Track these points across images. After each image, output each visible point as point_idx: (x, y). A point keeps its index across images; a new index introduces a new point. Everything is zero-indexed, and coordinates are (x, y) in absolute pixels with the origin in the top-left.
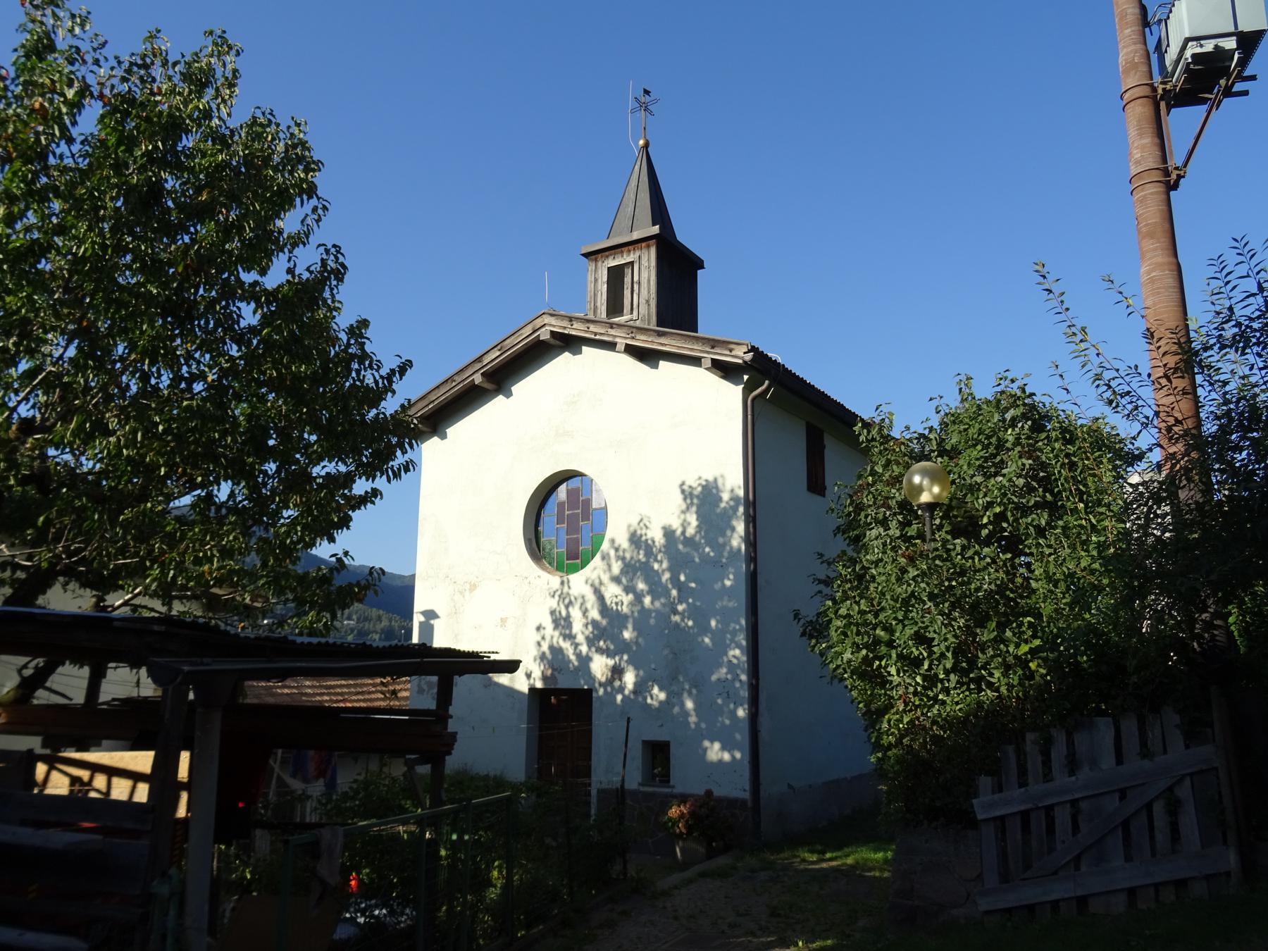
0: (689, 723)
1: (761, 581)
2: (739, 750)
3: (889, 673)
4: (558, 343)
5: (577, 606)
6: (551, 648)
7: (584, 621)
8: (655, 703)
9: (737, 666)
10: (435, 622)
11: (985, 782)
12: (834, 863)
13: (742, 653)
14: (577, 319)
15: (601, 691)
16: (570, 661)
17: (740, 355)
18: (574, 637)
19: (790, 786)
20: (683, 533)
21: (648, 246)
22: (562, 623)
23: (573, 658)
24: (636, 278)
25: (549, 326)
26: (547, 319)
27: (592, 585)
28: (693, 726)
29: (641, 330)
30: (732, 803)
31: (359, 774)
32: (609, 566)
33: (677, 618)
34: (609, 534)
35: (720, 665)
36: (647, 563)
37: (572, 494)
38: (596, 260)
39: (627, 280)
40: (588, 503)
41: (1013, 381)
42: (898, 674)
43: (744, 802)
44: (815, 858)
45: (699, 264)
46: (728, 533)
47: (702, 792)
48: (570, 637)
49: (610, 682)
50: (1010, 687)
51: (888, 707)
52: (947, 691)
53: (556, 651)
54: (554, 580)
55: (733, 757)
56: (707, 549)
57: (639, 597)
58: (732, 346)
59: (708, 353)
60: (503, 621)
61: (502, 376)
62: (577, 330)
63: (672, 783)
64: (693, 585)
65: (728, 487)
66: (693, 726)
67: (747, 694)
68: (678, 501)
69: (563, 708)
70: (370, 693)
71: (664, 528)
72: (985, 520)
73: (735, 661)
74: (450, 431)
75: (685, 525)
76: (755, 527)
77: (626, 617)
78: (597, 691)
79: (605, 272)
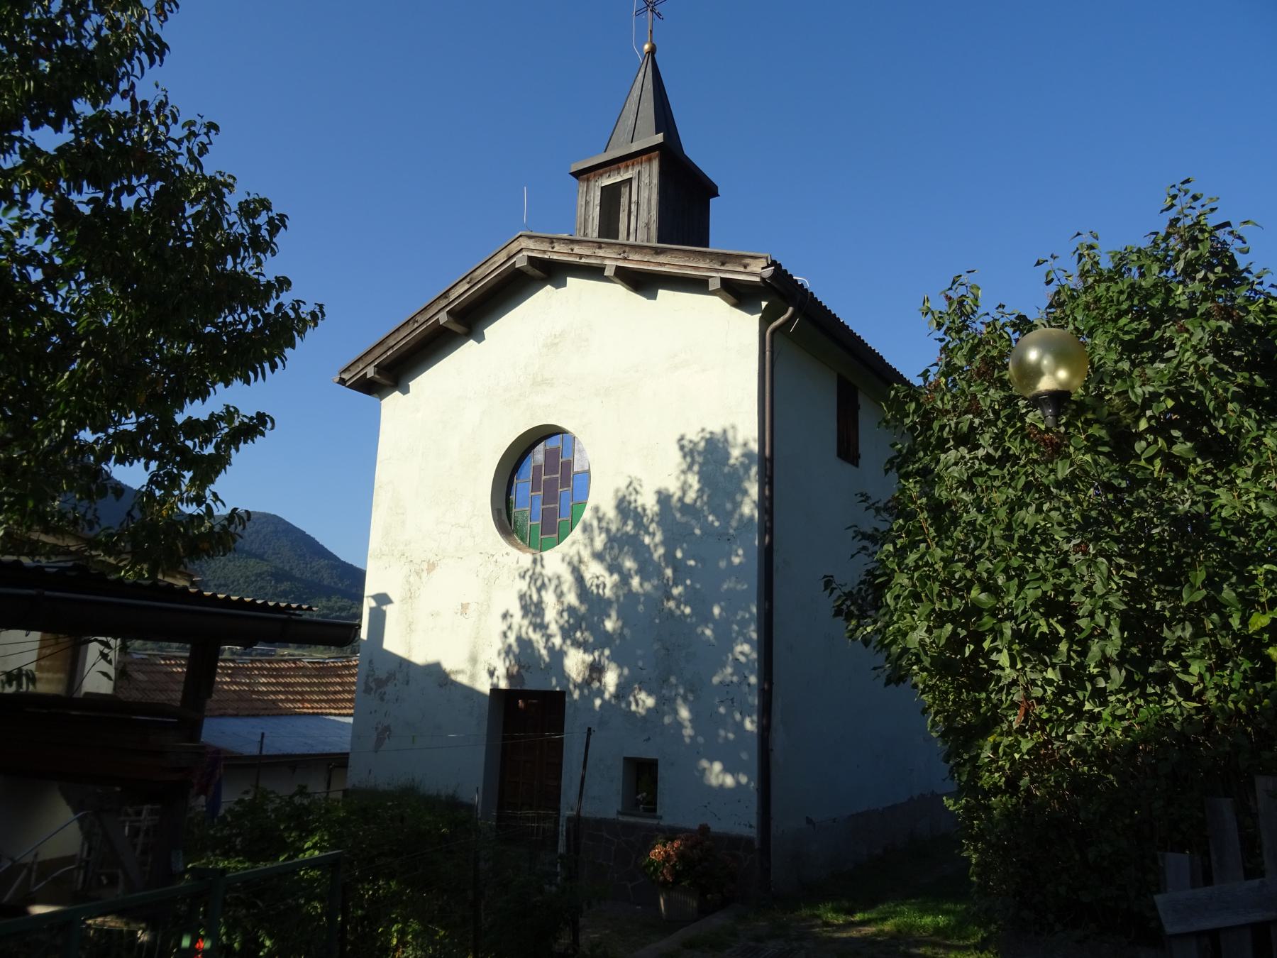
0: (683, 736)
3: (994, 665)
4: (537, 272)
5: (551, 589)
6: (519, 639)
7: (559, 607)
8: (642, 711)
10: (388, 609)
11: (1177, 864)
14: (559, 239)
15: (576, 695)
16: (540, 656)
17: (757, 271)
19: (809, 821)
20: (681, 499)
21: (650, 160)
22: (532, 609)
23: (544, 652)
24: (634, 198)
25: (527, 250)
26: (524, 243)
27: (569, 563)
28: (687, 740)
29: (635, 248)
30: (735, 843)
31: (246, 792)
32: (592, 540)
33: (672, 604)
34: (591, 503)
36: (636, 536)
37: (551, 455)
38: (588, 180)
39: (624, 201)
40: (568, 465)
41: (1195, 198)
42: (1013, 665)
43: (749, 841)
44: (841, 920)
45: (712, 191)
46: (738, 497)
48: (541, 627)
49: (587, 682)
50: (1225, 692)
51: (990, 722)
52: (1100, 696)
53: (525, 644)
54: (526, 559)
55: (738, 783)
56: (711, 518)
57: (625, 578)
58: (747, 261)
59: (717, 271)
60: (464, 607)
62: (559, 253)
63: (659, 813)
64: (692, 563)
65: (740, 440)
66: (687, 740)
67: (756, 702)
69: (528, 712)
70: (335, 693)
71: (659, 493)
72: (1143, 425)
73: (742, 659)
74: (489, 331)
75: (684, 488)
77: (609, 602)
78: (571, 694)
79: (598, 193)
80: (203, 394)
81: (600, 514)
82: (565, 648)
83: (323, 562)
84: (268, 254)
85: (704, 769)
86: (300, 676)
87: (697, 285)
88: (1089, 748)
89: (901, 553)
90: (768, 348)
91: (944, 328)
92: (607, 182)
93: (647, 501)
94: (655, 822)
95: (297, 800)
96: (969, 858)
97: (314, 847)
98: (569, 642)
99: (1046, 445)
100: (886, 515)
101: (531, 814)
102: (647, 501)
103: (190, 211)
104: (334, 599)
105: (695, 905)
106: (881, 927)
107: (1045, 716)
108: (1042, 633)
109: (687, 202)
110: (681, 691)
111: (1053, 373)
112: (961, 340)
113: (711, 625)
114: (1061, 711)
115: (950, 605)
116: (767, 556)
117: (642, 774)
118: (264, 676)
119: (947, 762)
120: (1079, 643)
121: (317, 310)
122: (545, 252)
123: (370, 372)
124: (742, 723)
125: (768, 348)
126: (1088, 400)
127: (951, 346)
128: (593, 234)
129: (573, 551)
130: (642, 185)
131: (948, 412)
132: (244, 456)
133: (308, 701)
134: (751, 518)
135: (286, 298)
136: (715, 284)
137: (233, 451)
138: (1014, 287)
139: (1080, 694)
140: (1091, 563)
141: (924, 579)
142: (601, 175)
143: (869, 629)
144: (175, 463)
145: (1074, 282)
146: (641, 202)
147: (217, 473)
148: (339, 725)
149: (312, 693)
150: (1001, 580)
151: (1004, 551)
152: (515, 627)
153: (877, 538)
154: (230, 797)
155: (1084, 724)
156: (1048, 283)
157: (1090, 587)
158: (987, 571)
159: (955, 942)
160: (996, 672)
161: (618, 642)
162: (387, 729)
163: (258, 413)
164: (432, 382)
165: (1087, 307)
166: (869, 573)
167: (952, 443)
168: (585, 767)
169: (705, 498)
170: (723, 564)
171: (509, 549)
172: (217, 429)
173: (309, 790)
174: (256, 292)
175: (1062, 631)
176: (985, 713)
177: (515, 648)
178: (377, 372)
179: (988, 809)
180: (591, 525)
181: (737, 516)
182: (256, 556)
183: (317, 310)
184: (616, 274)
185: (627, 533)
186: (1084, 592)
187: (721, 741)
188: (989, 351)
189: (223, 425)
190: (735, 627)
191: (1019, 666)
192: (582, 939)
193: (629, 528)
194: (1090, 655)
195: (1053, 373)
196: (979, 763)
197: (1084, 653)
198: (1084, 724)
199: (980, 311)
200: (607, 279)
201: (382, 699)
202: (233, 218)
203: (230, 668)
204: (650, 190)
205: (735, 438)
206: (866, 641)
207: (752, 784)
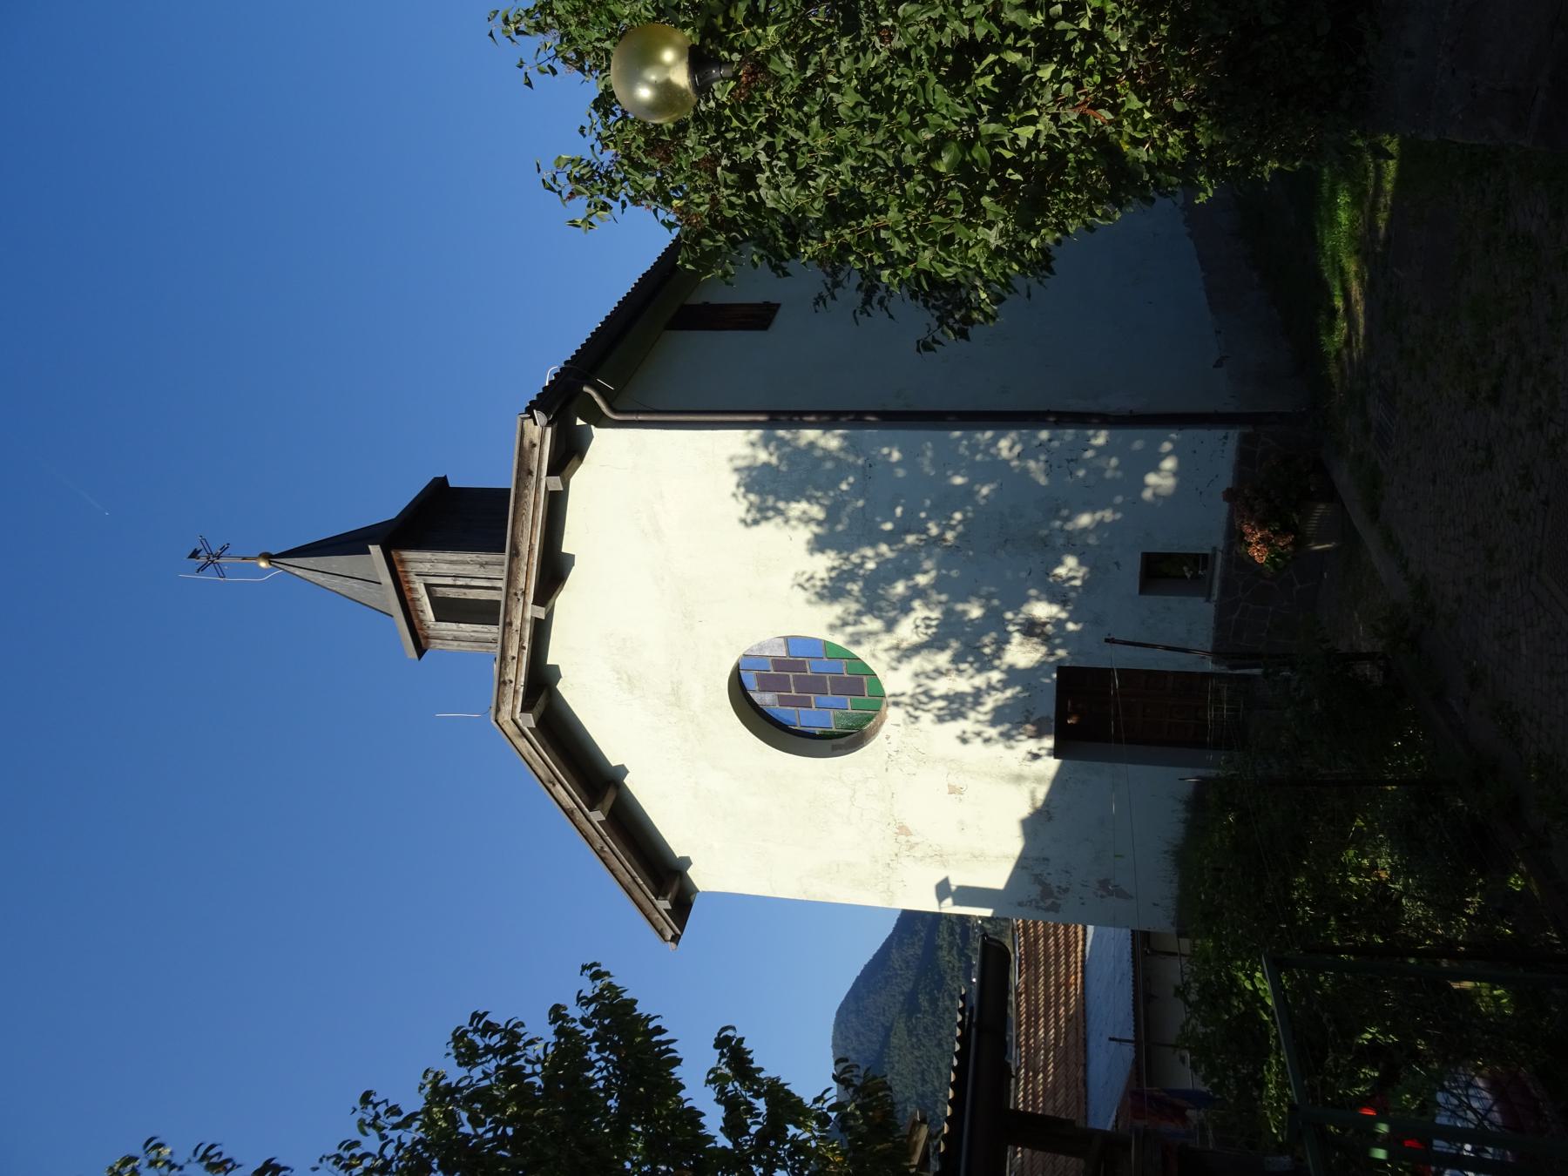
1: (894, 406)
2: (1160, 443)
3: (1033, 143)
4: (541, 701)
6: (993, 723)
7: (953, 675)
8: (1082, 572)
9: (1026, 444)
10: (955, 883)
12: (1356, 290)
13: (1003, 436)
15: (1061, 653)
16: (1014, 697)
17: (538, 431)
19: (1218, 364)
20: (820, 523)
21: (402, 562)
22: (956, 706)
23: (1009, 693)
24: (449, 581)
26: (505, 716)
27: (899, 660)
28: (1118, 516)
30: (1245, 458)
31: (1183, 1060)
32: (871, 634)
33: (950, 535)
34: (824, 635)
35: (1025, 471)
37: (766, 684)
38: (427, 637)
39: (453, 593)
40: (778, 663)
42: (1033, 121)
43: (1244, 439)
46: (818, 453)
47: (1226, 505)
48: (977, 696)
49: (1046, 640)
51: (1104, 147)
53: (998, 717)
54: (894, 715)
56: (844, 487)
57: (918, 593)
58: (526, 443)
59: (539, 480)
60: (953, 790)
61: (592, 777)
62: (518, 674)
63: (1208, 551)
64: (899, 511)
65: (748, 451)
66: (1118, 516)
68: (769, 530)
69: (1082, 712)
70: (1057, 945)
73: (1018, 449)
74: (614, 759)
75: (806, 520)
76: (809, 413)
77: (948, 613)
78: (1061, 660)
79: (443, 625)
80: (694, 1116)
81: (838, 623)
82: (1004, 667)
83: (895, 954)
84: (521, 1030)
85: (1155, 495)
86: (1037, 988)
87: (556, 506)
88: (1137, 24)
89: (893, 262)
90: (634, 418)
91: (609, 201)
92: (429, 614)
93: (823, 565)
94: (1219, 555)
95: (1193, 997)
96: (1271, 171)
97: (1251, 978)
98: (997, 662)
99: (754, 80)
100: (842, 276)
101: (1211, 714)
102: (823, 565)
103: (467, 1129)
104: (939, 942)
105: (1322, 506)
106: (1352, 275)
107: (1097, 78)
108: (994, 83)
109: (454, 516)
110: (1058, 523)
111: (667, 67)
112: (623, 181)
114: (1091, 60)
115: (957, 203)
116: (893, 418)
117: (1160, 571)
118: (1036, 1032)
119: (1153, 200)
120: (1004, 36)
121: (589, 973)
122: (516, 692)
123: (664, 905)
124: (1097, 448)
125: (634, 418)
126: (699, 24)
127: (632, 193)
128: (493, 631)
129: (885, 657)
130: (433, 571)
131: (713, 198)
132: (769, 1061)
133: (1068, 976)
134: (844, 437)
135: (575, 1012)
136: (556, 483)
137: (762, 1075)
138: (558, 114)
139: (1070, 36)
140: (905, 22)
141: (924, 232)
142: (421, 621)
143: (983, 296)
144: (776, 1147)
145: (552, 39)
146: (454, 572)
147: (789, 1093)
148: (1097, 944)
149: (1057, 973)
150: (926, 135)
151: (890, 131)
152: (978, 727)
153: (870, 286)
154: (1186, 1077)
155: (1106, 29)
156: (554, 72)
157: (935, 21)
158: (915, 152)
159: (1371, 182)
160: (1042, 141)
162: (1104, 884)
163: (716, 1047)
164: (676, 829)
165: (583, 24)
166: (914, 296)
167: (752, 193)
168: (1154, 646)
169: (819, 494)
170: (901, 473)
171: (881, 735)
172: (737, 1095)
173: (1178, 982)
174: (569, 1048)
175: (991, 58)
176: (1093, 154)
178: (665, 897)
179: (1211, 150)
180: (852, 635)
181: (842, 455)
182: (887, 1036)
183: (589, 973)
184: (542, 605)
185: (861, 590)
186: (940, 28)
187: (1119, 474)
188: (638, 147)
189: (730, 1088)
190: (979, 457)
191: (1035, 112)
192: (1365, 647)
193: (855, 588)
194: (1020, 23)
195: (667, 67)
196: (1155, 161)
197: (1020, 33)
198: (1106, 29)
199: (588, 156)
200: (550, 615)
201: (1066, 890)
202: (477, 1073)
203: (1026, 1074)
204: (439, 561)
205: (745, 458)
206: (998, 300)
207: (1173, 436)
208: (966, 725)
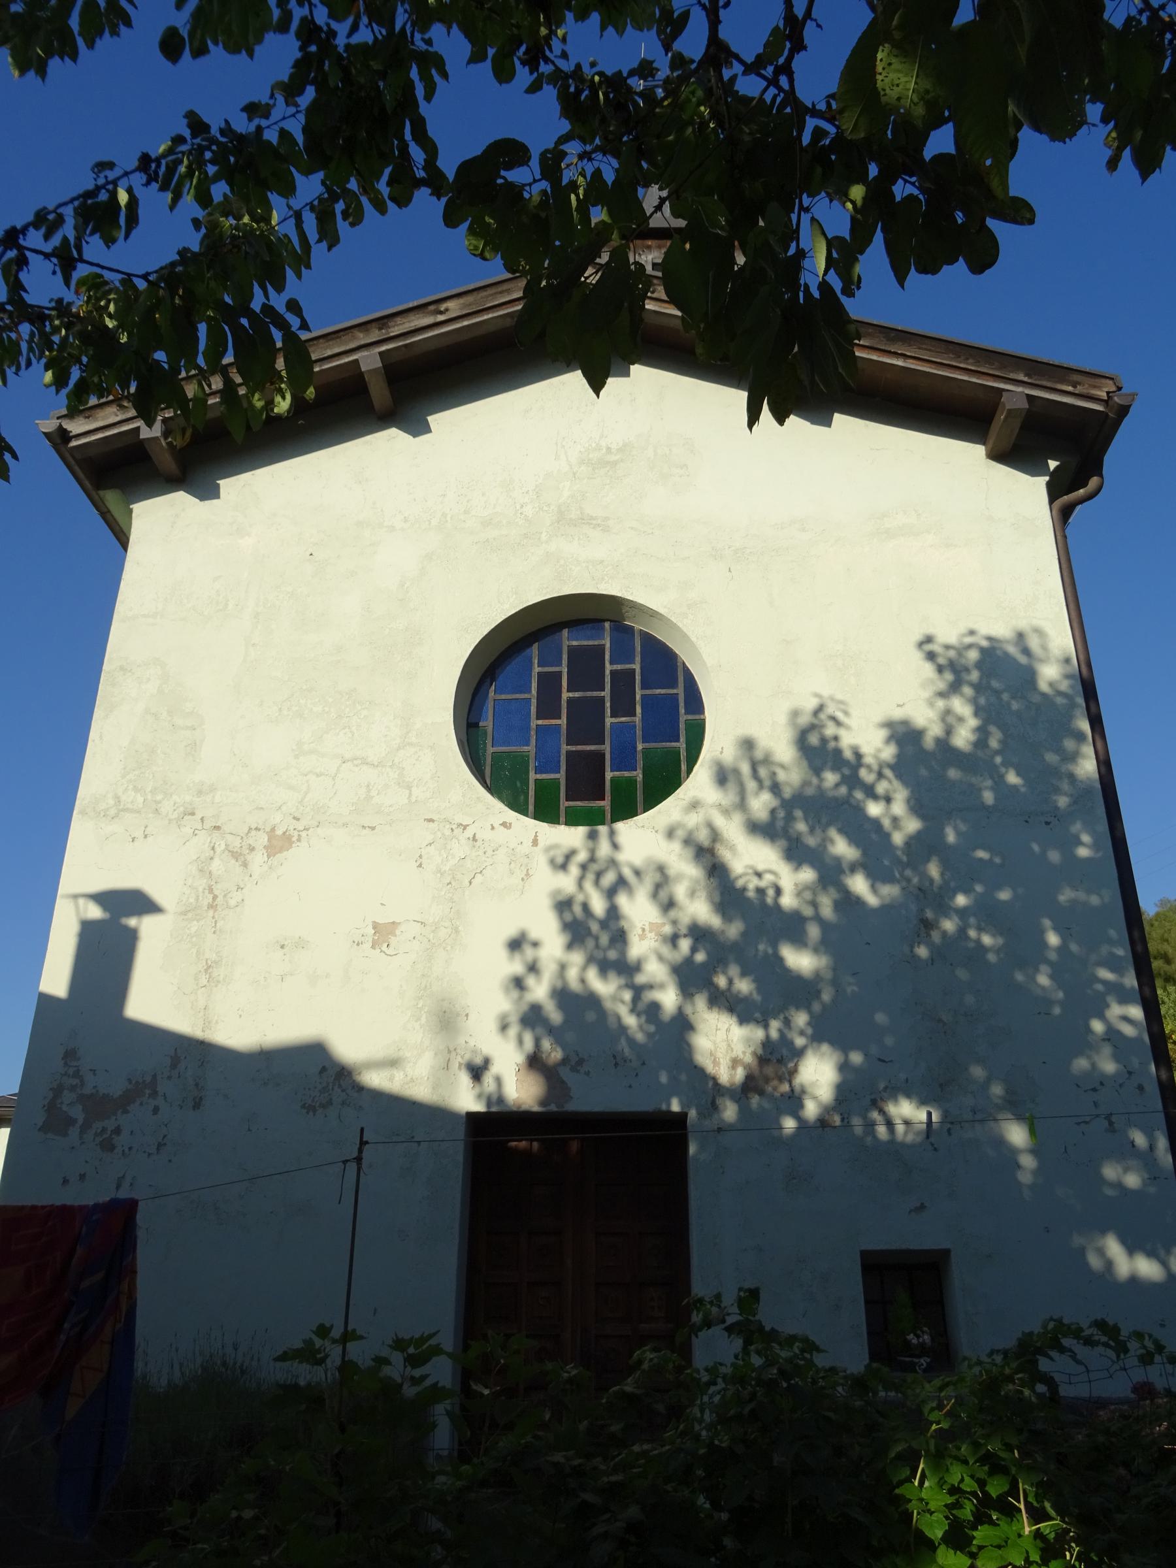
6: (562, 995)
10: (147, 927)
16: (623, 1029)
18: (637, 967)
23: (631, 1021)
27: (688, 841)
33: (949, 925)
48: (624, 968)
49: (751, 1085)
74: (229, 486)
75: (949, 720)
81: (759, 754)
102: (865, 737)
113: (1044, 968)
161: (826, 996)
177: (555, 1015)
180: (736, 772)
205: (1044, 648)
208: (552, 943)
